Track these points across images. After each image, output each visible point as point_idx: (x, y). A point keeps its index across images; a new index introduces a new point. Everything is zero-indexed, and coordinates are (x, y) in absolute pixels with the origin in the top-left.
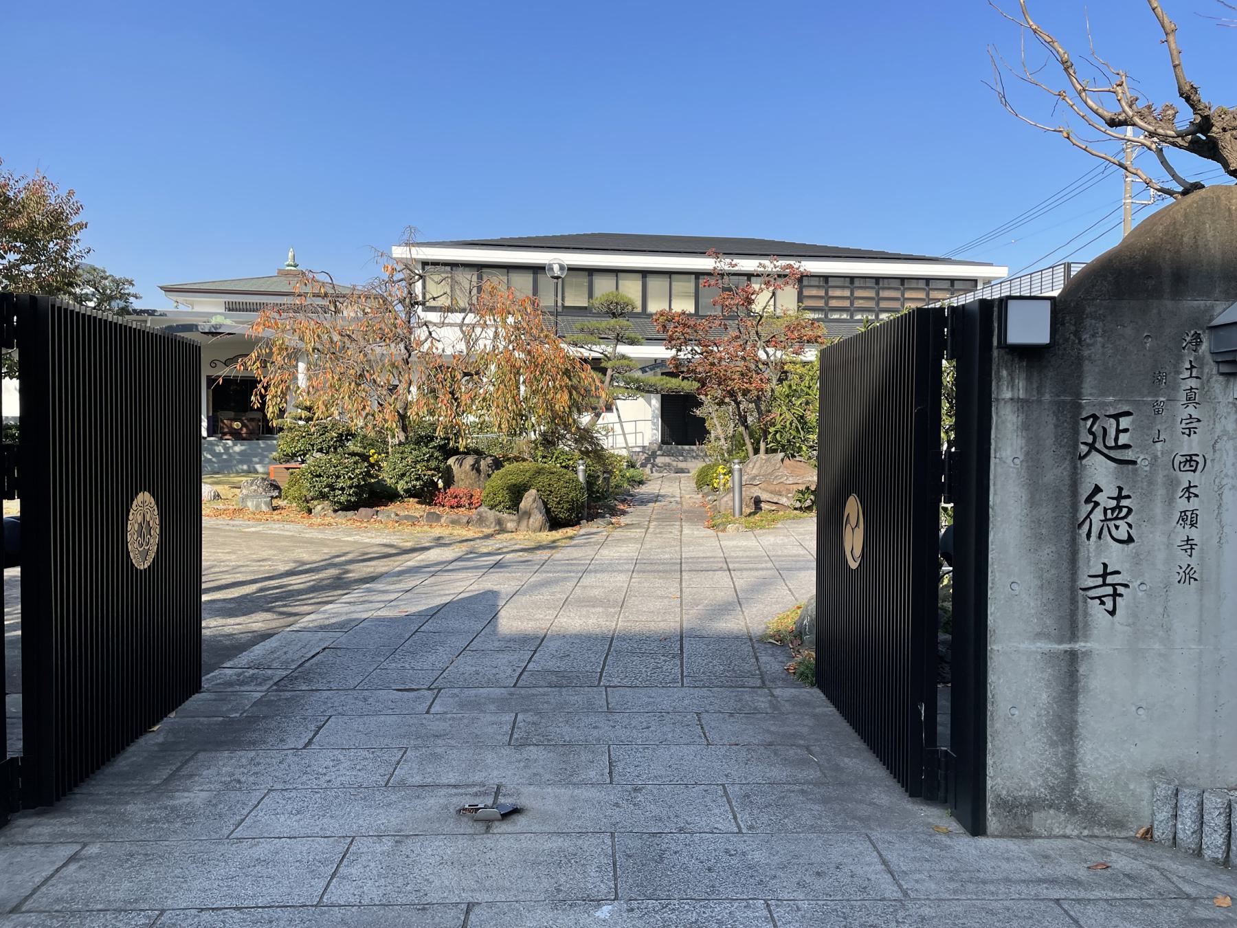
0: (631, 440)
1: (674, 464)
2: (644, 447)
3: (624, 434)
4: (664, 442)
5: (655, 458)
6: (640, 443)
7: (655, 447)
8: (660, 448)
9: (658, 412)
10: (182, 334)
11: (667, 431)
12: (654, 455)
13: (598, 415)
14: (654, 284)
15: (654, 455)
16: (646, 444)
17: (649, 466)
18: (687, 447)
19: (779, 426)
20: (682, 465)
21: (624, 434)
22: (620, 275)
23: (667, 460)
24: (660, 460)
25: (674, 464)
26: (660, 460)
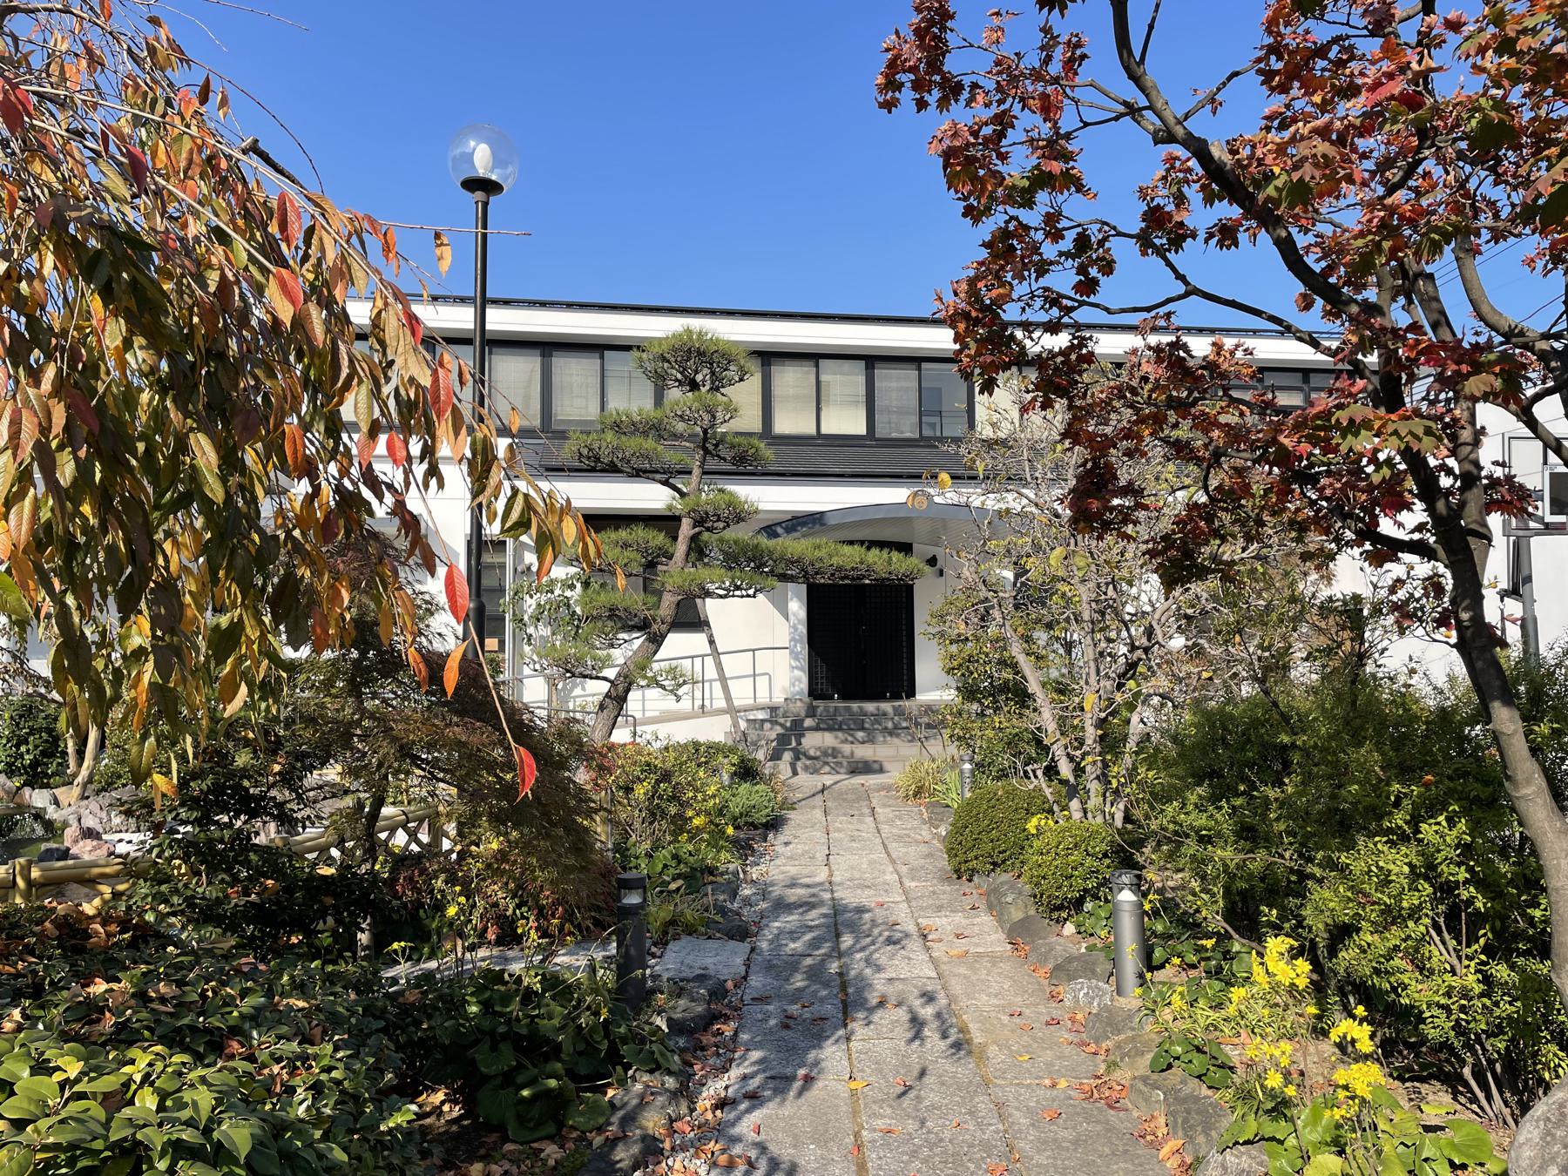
0: (742, 693)
1: (847, 748)
2: (773, 709)
3: (723, 680)
4: (814, 692)
5: (799, 737)
6: (763, 698)
7: (799, 708)
8: (811, 712)
9: (803, 629)
10: (394, 415)
11: (822, 670)
12: (797, 729)
13: (657, 640)
14: (789, 379)
15: (797, 729)
16: (779, 699)
17: (787, 756)
18: (870, 707)
19: (974, 978)
20: (864, 752)
21: (723, 680)
22: (822, 362)
23: (828, 739)
24: (813, 741)
25: (847, 748)
26: (813, 741)
